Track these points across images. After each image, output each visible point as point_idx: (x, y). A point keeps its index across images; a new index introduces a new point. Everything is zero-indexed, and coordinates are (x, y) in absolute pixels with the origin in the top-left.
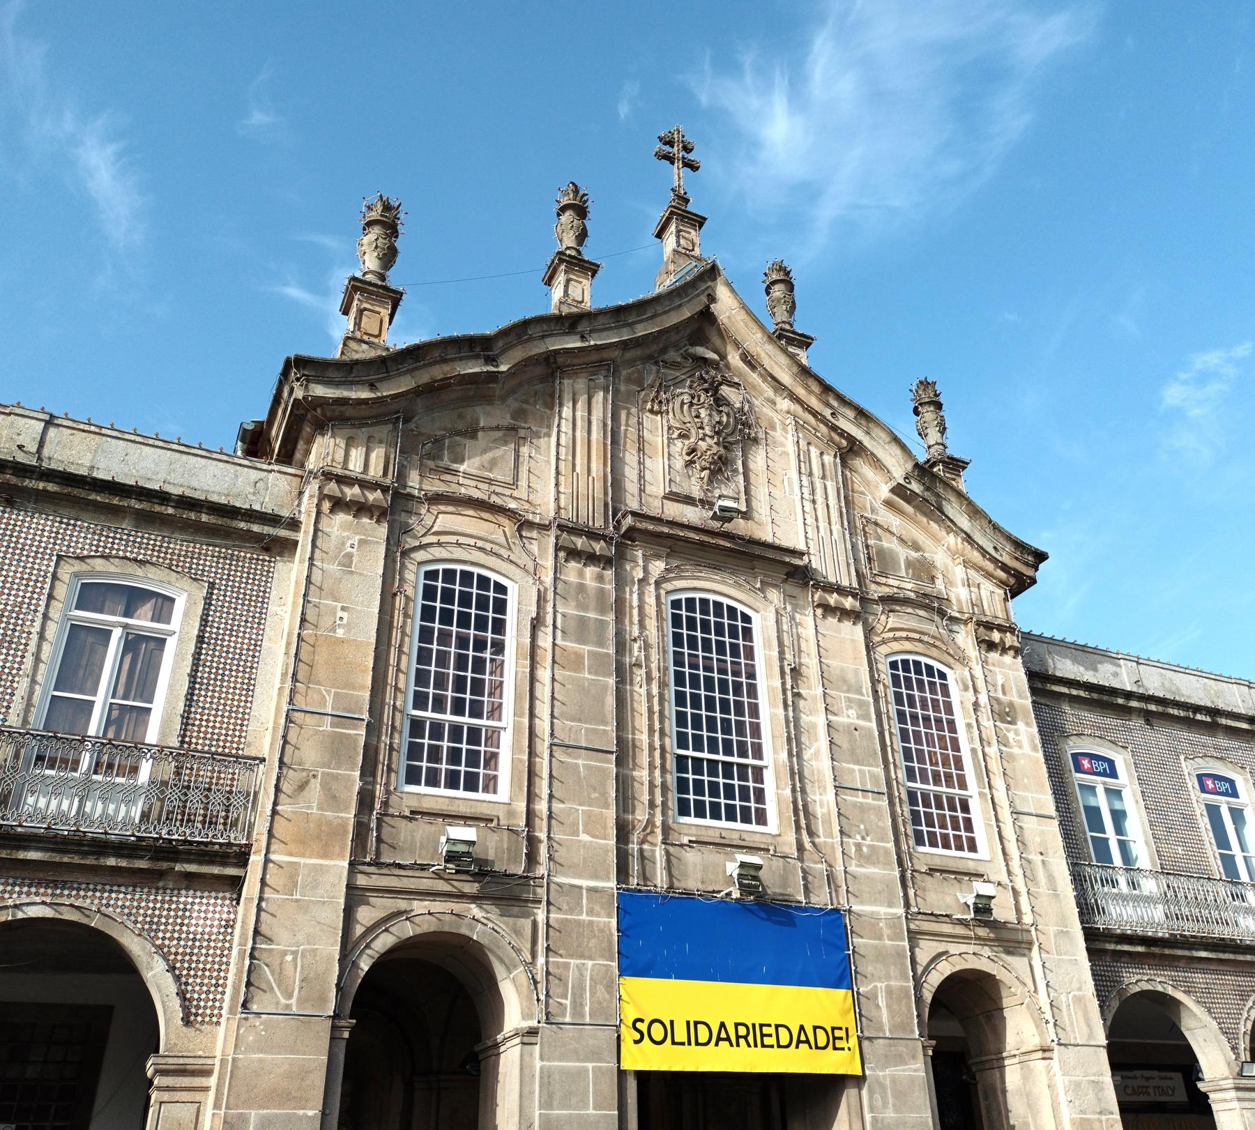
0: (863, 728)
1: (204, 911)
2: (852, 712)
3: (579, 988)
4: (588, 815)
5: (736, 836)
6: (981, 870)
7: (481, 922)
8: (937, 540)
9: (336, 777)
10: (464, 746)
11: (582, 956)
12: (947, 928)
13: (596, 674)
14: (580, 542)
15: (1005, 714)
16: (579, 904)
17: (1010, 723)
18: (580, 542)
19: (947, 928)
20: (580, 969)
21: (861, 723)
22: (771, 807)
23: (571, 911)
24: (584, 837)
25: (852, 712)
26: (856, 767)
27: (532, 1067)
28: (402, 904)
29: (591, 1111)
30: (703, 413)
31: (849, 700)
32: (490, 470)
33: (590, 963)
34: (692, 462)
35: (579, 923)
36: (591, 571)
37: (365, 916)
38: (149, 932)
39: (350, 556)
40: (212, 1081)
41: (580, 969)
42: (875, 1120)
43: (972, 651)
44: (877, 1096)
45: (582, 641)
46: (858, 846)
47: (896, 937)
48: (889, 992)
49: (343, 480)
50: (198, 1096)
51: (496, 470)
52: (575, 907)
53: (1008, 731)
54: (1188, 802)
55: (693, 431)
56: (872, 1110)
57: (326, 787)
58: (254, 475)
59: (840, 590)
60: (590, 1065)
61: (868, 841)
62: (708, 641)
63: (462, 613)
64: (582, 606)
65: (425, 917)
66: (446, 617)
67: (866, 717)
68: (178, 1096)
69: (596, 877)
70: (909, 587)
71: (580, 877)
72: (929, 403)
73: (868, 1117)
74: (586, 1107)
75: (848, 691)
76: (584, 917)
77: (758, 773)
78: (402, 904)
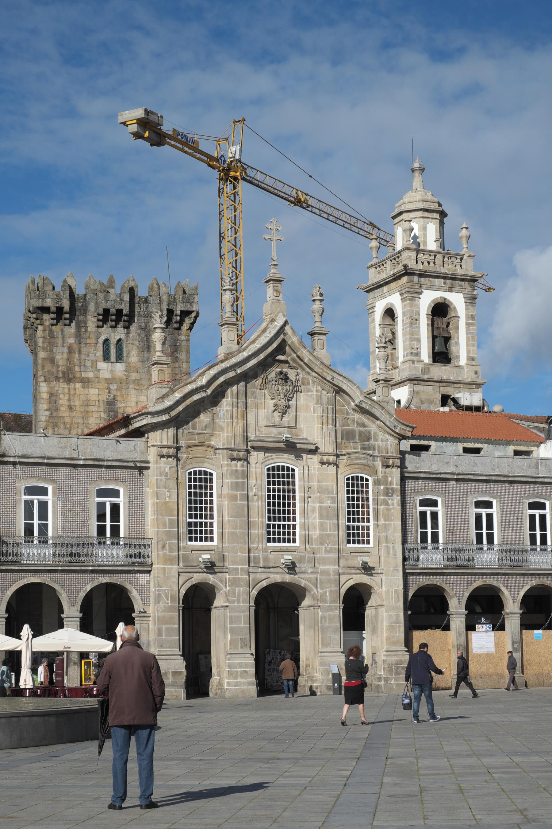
0: (332, 507)
1: (143, 578)
2: (329, 502)
3: (239, 595)
4: (240, 547)
5: (285, 548)
6: (369, 551)
7: (211, 579)
8: (374, 423)
9: (172, 543)
10: (198, 498)
11: (239, 587)
12: (353, 571)
13: (242, 501)
14: (235, 453)
15: (388, 493)
16: (238, 573)
17: (390, 496)
18: (235, 453)
19: (353, 571)
20: (239, 590)
21: (332, 505)
22: (298, 537)
23: (236, 575)
24: (239, 554)
25: (329, 502)
26: (328, 521)
27: (227, 615)
28: (191, 575)
29: (242, 625)
30: (280, 388)
31: (328, 497)
32: (205, 430)
33: (241, 588)
34: (275, 410)
35: (238, 578)
36: (240, 463)
37: (182, 579)
38: (131, 583)
39: (167, 473)
40: (151, 618)
41: (239, 590)
42: (322, 627)
43: (380, 469)
44: (323, 620)
45: (237, 490)
46: (326, 548)
47: (335, 575)
48: (331, 591)
49: (162, 447)
50: (148, 622)
51: (207, 430)
52: (237, 573)
53: (389, 499)
54: (467, 514)
55: (276, 397)
56: (321, 623)
57: (170, 546)
58: (134, 443)
59: (329, 455)
60: (242, 614)
61: (330, 546)
62: (280, 478)
63: (200, 483)
64: (237, 478)
65: (197, 578)
66: (195, 487)
67: (333, 503)
68: (144, 622)
69: (243, 565)
70: (447, 281)
71: (238, 565)
72: (425, 251)
73: (320, 625)
74: (241, 624)
75: (328, 494)
76: (240, 576)
77: (294, 527)
78: (191, 575)
